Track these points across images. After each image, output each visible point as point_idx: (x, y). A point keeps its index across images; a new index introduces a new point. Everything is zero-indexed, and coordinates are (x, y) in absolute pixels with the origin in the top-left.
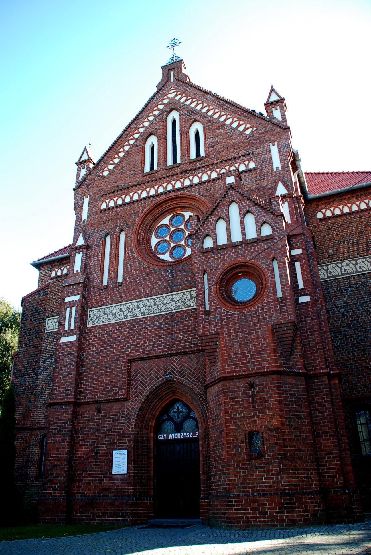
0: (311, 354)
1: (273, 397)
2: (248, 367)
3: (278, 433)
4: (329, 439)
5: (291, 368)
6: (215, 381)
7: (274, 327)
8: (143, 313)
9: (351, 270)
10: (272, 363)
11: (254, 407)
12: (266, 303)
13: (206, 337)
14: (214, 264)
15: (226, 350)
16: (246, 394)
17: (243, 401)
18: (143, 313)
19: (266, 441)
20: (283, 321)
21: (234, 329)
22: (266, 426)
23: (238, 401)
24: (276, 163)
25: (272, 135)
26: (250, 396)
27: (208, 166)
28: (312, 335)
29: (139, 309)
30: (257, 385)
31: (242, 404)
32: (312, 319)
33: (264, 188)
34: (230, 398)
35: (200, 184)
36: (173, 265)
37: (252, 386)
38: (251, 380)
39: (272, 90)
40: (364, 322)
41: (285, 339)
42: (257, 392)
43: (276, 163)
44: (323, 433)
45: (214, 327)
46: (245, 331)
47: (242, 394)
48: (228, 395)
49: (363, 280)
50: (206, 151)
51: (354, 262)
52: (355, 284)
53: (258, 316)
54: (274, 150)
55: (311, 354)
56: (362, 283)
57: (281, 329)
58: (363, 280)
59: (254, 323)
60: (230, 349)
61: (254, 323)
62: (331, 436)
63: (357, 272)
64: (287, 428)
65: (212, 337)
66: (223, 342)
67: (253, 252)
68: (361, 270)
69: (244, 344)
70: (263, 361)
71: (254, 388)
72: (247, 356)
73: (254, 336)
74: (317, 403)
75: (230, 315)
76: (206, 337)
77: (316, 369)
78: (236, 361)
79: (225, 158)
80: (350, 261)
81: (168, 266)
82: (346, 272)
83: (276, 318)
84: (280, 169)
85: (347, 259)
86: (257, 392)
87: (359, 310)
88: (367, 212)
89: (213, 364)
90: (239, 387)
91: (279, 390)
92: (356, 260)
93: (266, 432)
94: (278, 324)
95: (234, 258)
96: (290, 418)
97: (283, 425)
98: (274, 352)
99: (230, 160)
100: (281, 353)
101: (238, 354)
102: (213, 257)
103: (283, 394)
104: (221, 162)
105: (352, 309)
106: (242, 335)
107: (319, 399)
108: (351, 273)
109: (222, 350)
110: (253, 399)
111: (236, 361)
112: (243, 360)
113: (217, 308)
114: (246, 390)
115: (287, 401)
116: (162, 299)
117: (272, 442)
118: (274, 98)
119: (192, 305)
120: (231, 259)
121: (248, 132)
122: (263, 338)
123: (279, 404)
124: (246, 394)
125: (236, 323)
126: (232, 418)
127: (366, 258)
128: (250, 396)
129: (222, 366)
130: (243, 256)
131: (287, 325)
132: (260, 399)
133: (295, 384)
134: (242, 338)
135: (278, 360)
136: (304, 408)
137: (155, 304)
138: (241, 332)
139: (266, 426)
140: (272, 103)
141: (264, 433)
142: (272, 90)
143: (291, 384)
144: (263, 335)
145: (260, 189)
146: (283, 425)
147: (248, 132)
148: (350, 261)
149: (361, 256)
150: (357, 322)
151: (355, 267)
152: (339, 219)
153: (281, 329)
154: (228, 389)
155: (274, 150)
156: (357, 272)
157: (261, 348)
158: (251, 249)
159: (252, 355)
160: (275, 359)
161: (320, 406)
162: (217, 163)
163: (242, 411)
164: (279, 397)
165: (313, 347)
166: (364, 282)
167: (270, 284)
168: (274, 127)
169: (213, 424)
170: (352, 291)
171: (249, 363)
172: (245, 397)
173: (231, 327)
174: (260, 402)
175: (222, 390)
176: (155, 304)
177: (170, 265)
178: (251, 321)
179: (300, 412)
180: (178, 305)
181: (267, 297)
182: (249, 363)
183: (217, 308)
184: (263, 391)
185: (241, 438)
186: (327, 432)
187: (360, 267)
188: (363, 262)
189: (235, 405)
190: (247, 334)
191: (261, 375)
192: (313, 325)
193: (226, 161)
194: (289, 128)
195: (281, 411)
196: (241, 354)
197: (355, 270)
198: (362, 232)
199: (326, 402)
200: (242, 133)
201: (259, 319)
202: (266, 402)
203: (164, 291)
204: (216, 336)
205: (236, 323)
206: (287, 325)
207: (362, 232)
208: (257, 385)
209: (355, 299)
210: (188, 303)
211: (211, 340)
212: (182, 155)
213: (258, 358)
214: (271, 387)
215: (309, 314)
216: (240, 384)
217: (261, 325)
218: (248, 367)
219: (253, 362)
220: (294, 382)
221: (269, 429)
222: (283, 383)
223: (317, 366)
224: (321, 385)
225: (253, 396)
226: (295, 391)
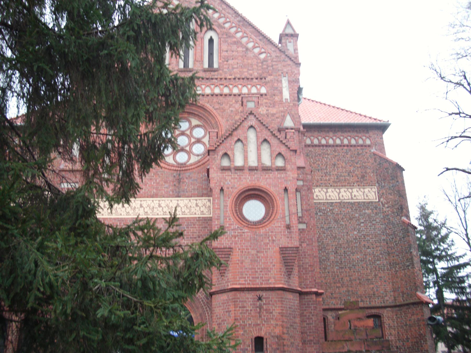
0: (304, 274)
1: (277, 310)
2: (258, 281)
3: (279, 340)
4: (313, 346)
5: (290, 285)
6: (225, 290)
7: (282, 249)
8: (147, 212)
9: (322, 197)
10: (278, 280)
11: (260, 316)
12: (276, 227)
13: (219, 250)
14: (231, 183)
15: (238, 264)
16: (254, 304)
17: (251, 310)
18: (147, 212)
19: (269, 346)
20: (290, 246)
21: (246, 246)
22: (270, 333)
23: (247, 310)
24: (286, 94)
25: (284, 66)
26: (257, 307)
27: (221, 79)
28: (306, 258)
29: (142, 209)
30: (265, 298)
31: (251, 313)
32: (307, 245)
33: (273, 115)
34: (240, 307)
35: (212, 95)
36: (180, 171)
37: (260, 299)
38: (259, 293)
39: (288, 23)
40: (328, 245)
41: (289, 261)
42: (264, 304)
43: (286, 94)
44: (308, 341)
45: (228, 241)
46: (256, 249)
47: (251, 304)
48: (238, 304)
49: (331, 208)
50: (219, 63)
51: (325, 190)
52: (324, 210)
53: (269, 238)
54: (285, 83)
55: (304, 274)
56: (330, 210)
57: (287, 252)
58: (331, 208)
59: (264, 243)
60: (242, 263)
61: (264, 243)
62: (314, 343)
63: (326, 199)
64: (286, 336)
65: (225, 250)
66: (236, 256)
67: (267, 178)
68: (330, 198)
69: (255, 261)
70: (271, 278)
71: (261, 300)
72: (257, 272)
73: (264, 254)
74: (306, 316)
75: (244, 233)
76: (219, 250)
77: (307, 288)
78: (247, 275)
79: (238, 76)
80: (322, 189)
81: (175, 170)
82: (317, 198)
83: (284, 242)
84: (289, 101)
85: (320, 186)
86: (264, 304)
87: (324, 233)
88: (341, 148)
89: (223, 274)
90: (248, 298)
91: (282, 304)
92: (327, 189)
93: (269, 338)
94: (285, 248)
95: (250, 181)
96: (289, 328)
97: (283, 333)
98: (280, 271)
99: (243, 79)
100: (285, 273)
101: (249, 269)
102: (230, 176)
103: (284, 307)
104: (235, 79)
105: (319, 232)
106: (254, 252)
107: (307, 313)
108: (321, 200)
109: (235, 263)
110: (260, 309)
111: (247, 275)
112: (253, 275)
113: (231, 224)
114: (255, 301)
115: (287, 313)
116: (168, 202)
117: (274, 346)
118: (289, 31)
119: (197, 213)
120: (247, 181)
121: (263, 56)
122: (271, 257)
123: (282, 316)
124: (254, 304)
125: (248, 241)
126: (241, 325)
127: (335, 189)
128: (257, 307)
129: (234, 278)
130: (258, 180)
131: (292, 249)
132: (266, 310)
133: (293, 300)
134: (253, 255)
135: (283, 278)
136: (298, 320)
137: (160, 206)
138: (253, 249)
139: (270, 333)
140: (287, 35)
141: (268, 340)
142: (288, 23)
143: (290, 299)
144: (272, 256)
145: (269, 116)
146: (283, 333)
147: (263, 56)
148: (322, 189)
149: (331, 186)
150: (322, 244)
151: (326, 194)
152: (317, 148)
153: (287, 252)
154: (238, 298)
155: (285, 83)
156: (326, 199)
157: (269, 266)
158: (266, 176)
159: (261, 272)
160: (281, 277)
161: (308, 319)
162: (230, 79)
163: (250, 319)
164: (282, 310)
165: (306, 268)
166: (332, 210)
167: (280, 211)
168: (287, 59)
169: (219, 327)
170: (320, 215)
171: (258, 278)
172: (253, 307)
173: (244, 244)
174: (266, 313)
175: (232, 299)
176: (160, 206)
177: (177, 170)
178: (262, 241)
179: (295, 323)
180: (183, 211)
181: (278, 222)
182: (258, 278)
183: (231, 224)
184: (269, 304)
185: (248, 342)
186: (311, 341)
187: (330, 196)
188: (332, 192)
189: (245, 313)
190: (257, 252)
191: (268, 290)
192: (307, 250)
193: (239, 79)
194: (300, 64)
195: (283, 322)
196: (252, 269)
197: (325, 198)
198: (334, 165)
199: (313, 315)
200: (256, 57)
201: (269, 240)
202: (271, 313)
203: (170, 195)
204: (230, 250)
205: (248, 241)
206: (292, 249)
207: (334, 165)
208: (265, 298)
209: (322, 223)
210: (193, 210)
211: (224, 253)
212: (195, 61)
213: (266, 274)
214: (276, 301)
215: (305, 240)
216: (250, 296)
217: (270, 246)
218: (258, 281)
219: (262, 278)
220: (292, 297)
221: (273, 336)
222: (285, 299)
223: (308, 285)
224: (310, 301)
225: (261, 307)
226: (292, 305)
